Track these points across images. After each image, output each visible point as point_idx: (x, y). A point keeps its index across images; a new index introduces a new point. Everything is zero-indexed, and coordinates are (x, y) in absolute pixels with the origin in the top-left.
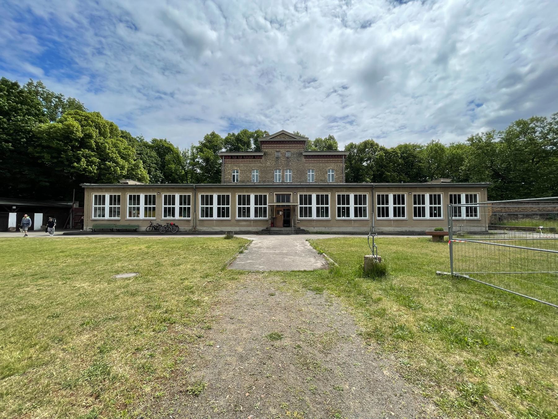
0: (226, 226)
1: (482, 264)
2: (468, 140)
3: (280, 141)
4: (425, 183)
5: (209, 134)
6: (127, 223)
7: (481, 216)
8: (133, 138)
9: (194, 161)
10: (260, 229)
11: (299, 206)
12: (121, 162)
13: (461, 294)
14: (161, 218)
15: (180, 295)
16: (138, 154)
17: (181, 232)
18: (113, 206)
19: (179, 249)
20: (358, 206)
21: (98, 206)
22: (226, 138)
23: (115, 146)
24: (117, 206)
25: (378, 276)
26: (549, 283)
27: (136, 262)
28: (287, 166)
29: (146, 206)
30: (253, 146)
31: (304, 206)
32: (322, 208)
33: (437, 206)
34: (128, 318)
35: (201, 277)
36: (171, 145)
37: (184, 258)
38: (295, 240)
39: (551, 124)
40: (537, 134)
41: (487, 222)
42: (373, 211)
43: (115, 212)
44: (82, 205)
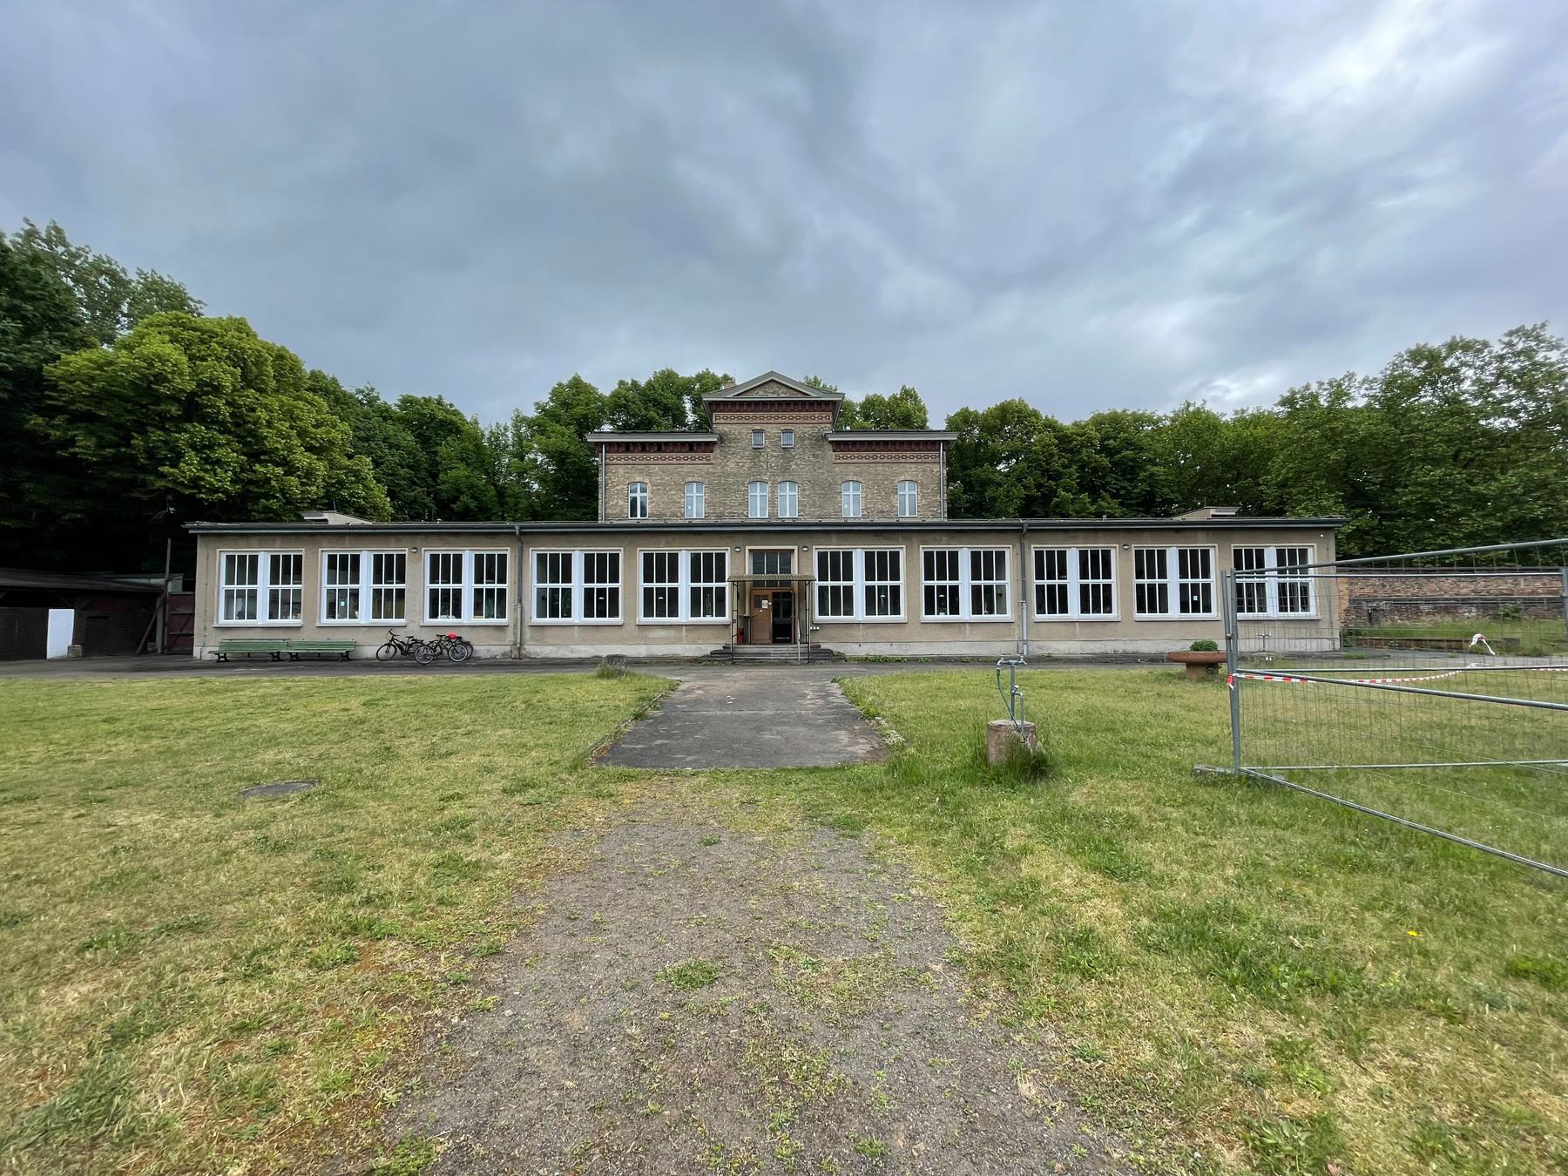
0: (610, 642)
1: (1320, 742)
2: (1283, 403)
3: (765, 403)
4: (1168, 520)
5: (565, 382)
6: (321, 637)
7: (1320, 608)
8: (344, 393)
9: (522, 459)
10: (707, 649)
11: (818, 583)
12: (303, 459)
13: (1263, 831)
14: (418, 622)
15: (427, 846)
16: (360, 439)
17: (478, 659)
18: (280, 587)
19: (461, 708)
20: (983, 582)
21: (235, 587)
22: (615, 395)
23: (290, 415)
24: (292, 586)
25: (1027, 780)
26: (1508, 794)
27: (323, 748)
28: (785, 474)
29: (378, 586)
30: (691, 418)
31: (830, 583)
32: (882, 589)
33: (1200, 581)
34: (240, 925)
35: (504, 791)
36: (456, 413)
37: (469, 733)
38: (804, 678)
39: (1502, 358)
40: (1466, 385)
41: (1338, 626)
42: (1024, 598)
43: (286, 603)
44: (190, 585)
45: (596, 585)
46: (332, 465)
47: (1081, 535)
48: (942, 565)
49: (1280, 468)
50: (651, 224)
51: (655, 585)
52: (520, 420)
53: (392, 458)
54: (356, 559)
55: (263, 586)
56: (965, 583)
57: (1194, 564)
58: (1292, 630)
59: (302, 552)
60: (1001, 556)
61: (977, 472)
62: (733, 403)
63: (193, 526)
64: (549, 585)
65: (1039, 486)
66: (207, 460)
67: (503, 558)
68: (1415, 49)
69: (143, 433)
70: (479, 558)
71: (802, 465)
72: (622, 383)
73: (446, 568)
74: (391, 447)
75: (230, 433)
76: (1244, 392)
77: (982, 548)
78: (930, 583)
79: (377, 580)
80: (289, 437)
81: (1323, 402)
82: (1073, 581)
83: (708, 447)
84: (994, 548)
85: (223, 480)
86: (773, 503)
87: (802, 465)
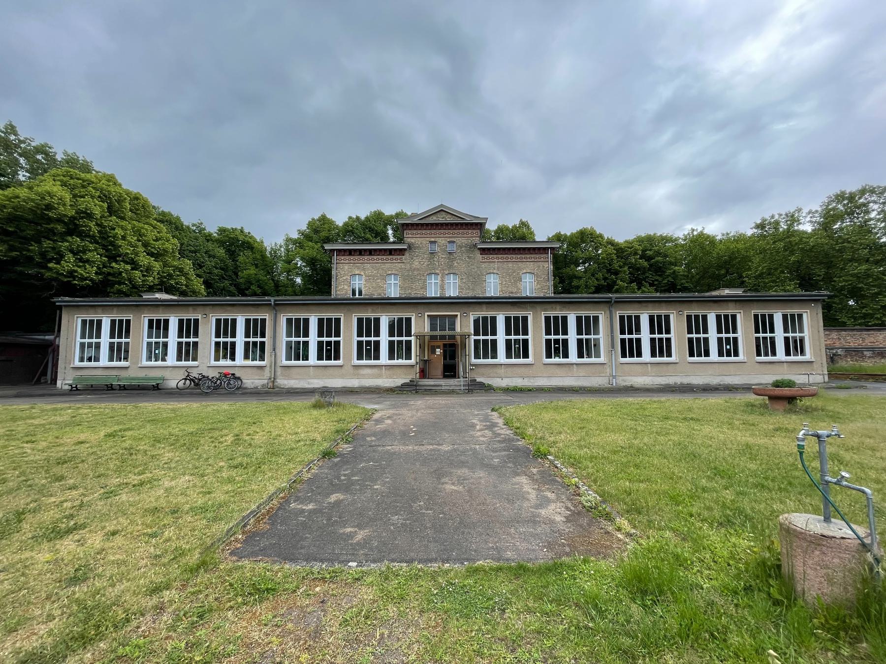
3: (437, 224)
5: (316, 218)
6: (142, 374)
10: (399, 382)
11: (473, 338)
12: (144, 260)
14: (207, 363)
17: (246, 388)
18: (116, 340)
21: (87, 340)
23: (139, 234)
31: (481, 337)
36: (251, 237)
38: (469, 406)
40: (873, 215)
42: (613, 347)
45: (325, 339)
46: (165, 265)
47: (650, 305)
48: (556, 325)
49: (757, 265)
50: (367, 140)
51: (364, 339)
52: (289, 240)
53: (209, 263)
54: (166, 322)
55: (105, 340)
56: (572, 337)
57: (727, 324)
58: (796, 368)
59: (131, 317)
60: (596, 319)
61: (567, 271)
62: (417, 225)
63: (60, 300)
64: (294, 339)
65: (605, 279)
66: (81, 260)
67: (263, 321)
68: (790, 42)
69: (39, 242)
70: (248, 321)
71: (461, 265)
72: (350, 218)
73: (225, 328)
74: (210, 256)
75: (97, 243)
76: (726, 226)
77: (583, 313)
78: (549, 337)
79: (180, 335)
80: (137, 246)
81: (783, 226)
82: (645, 336)
83: (401, 252)
84: (592, 313)
85: (91, 272)
86: (442, 288)
87: (461, 265)
